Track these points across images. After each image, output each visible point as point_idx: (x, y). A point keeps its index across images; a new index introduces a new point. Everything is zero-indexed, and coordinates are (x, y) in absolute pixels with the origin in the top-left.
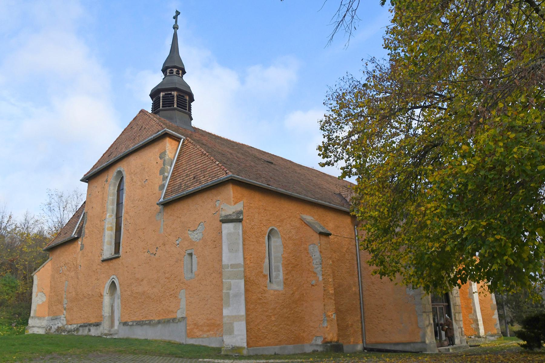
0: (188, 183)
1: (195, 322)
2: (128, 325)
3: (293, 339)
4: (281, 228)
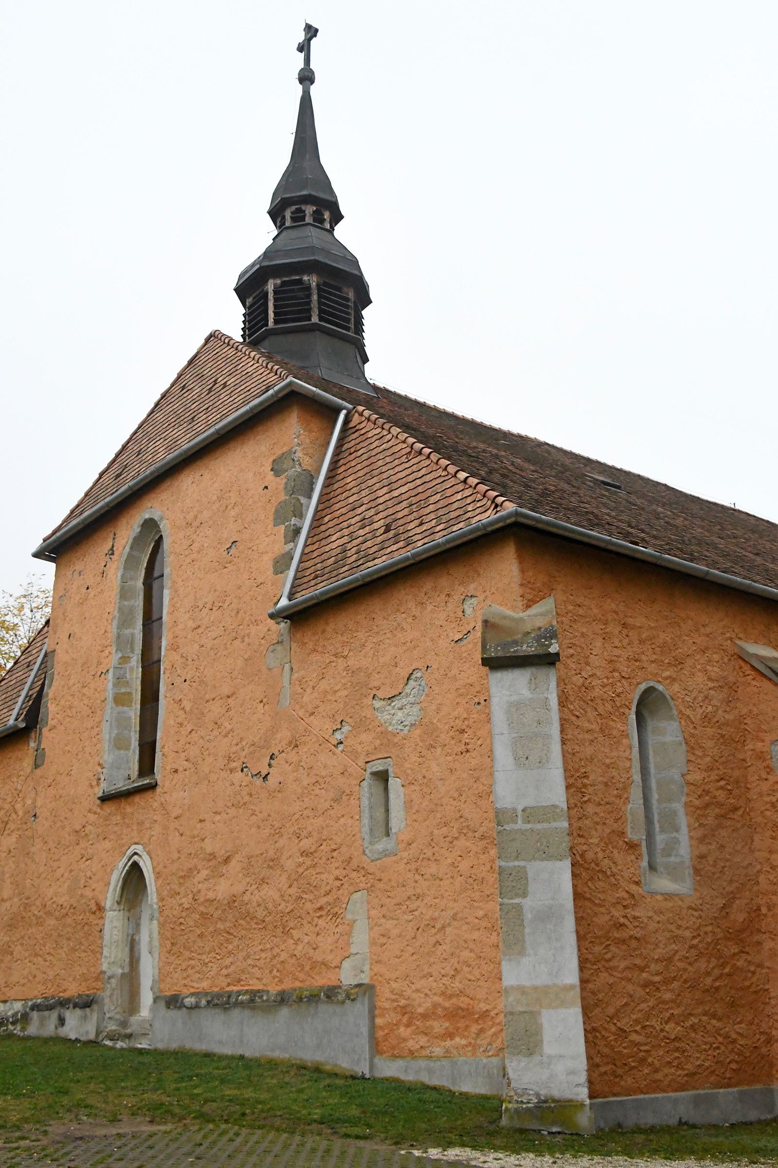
0: (369, 544)
1: (403, 1002)
2: (182, 1006)
3: (734, 1066)
4: (676, 687)
